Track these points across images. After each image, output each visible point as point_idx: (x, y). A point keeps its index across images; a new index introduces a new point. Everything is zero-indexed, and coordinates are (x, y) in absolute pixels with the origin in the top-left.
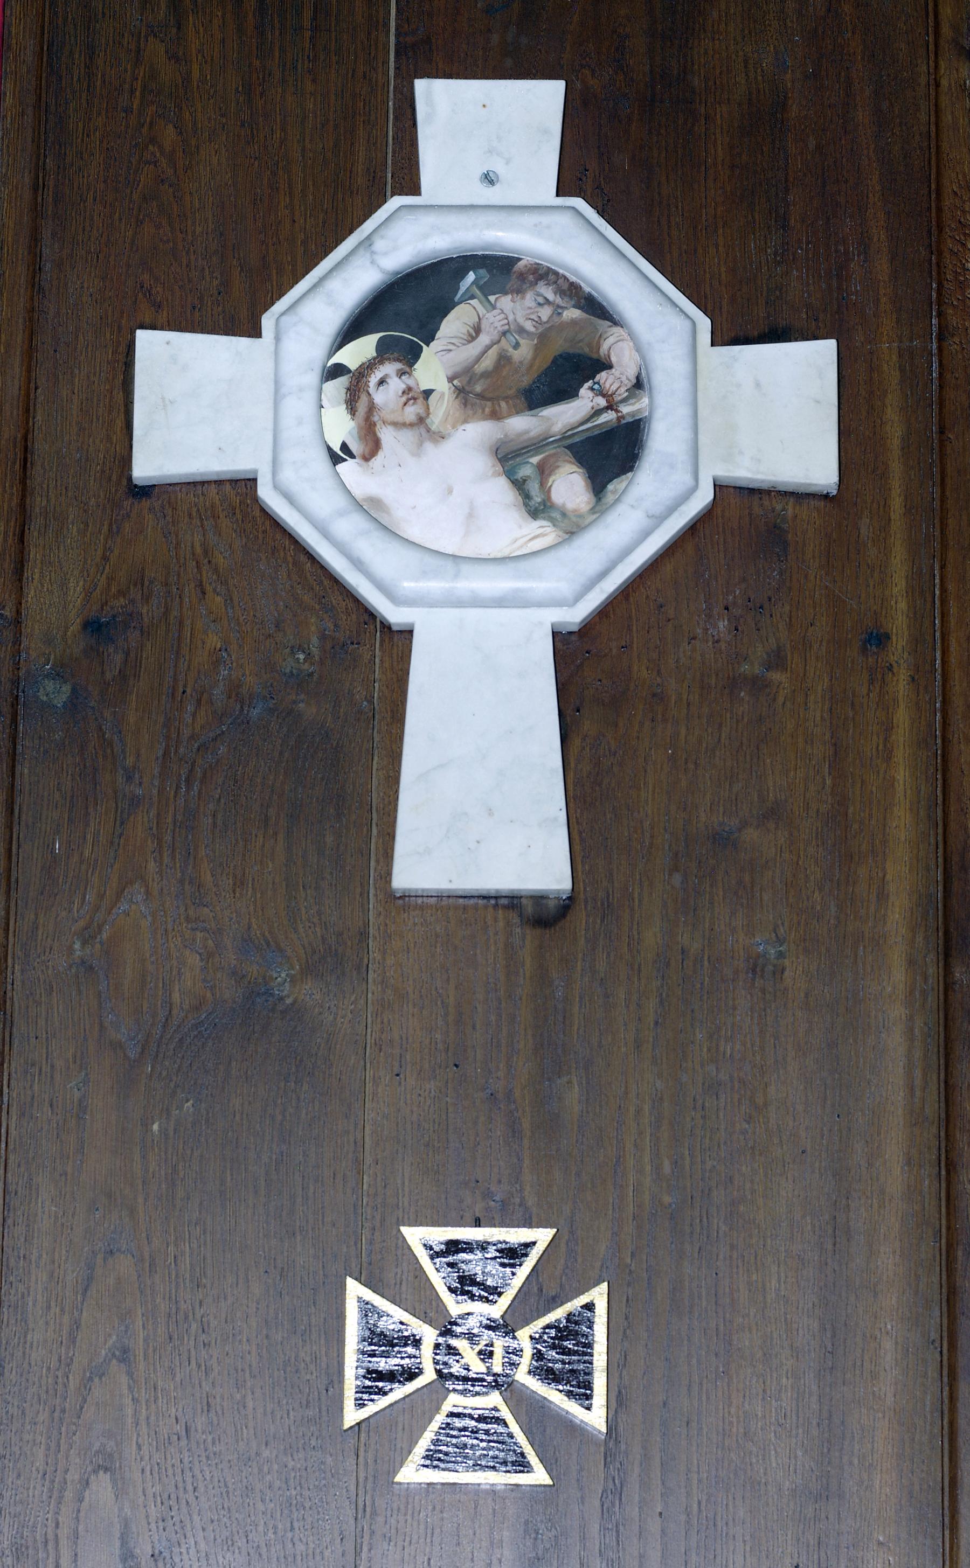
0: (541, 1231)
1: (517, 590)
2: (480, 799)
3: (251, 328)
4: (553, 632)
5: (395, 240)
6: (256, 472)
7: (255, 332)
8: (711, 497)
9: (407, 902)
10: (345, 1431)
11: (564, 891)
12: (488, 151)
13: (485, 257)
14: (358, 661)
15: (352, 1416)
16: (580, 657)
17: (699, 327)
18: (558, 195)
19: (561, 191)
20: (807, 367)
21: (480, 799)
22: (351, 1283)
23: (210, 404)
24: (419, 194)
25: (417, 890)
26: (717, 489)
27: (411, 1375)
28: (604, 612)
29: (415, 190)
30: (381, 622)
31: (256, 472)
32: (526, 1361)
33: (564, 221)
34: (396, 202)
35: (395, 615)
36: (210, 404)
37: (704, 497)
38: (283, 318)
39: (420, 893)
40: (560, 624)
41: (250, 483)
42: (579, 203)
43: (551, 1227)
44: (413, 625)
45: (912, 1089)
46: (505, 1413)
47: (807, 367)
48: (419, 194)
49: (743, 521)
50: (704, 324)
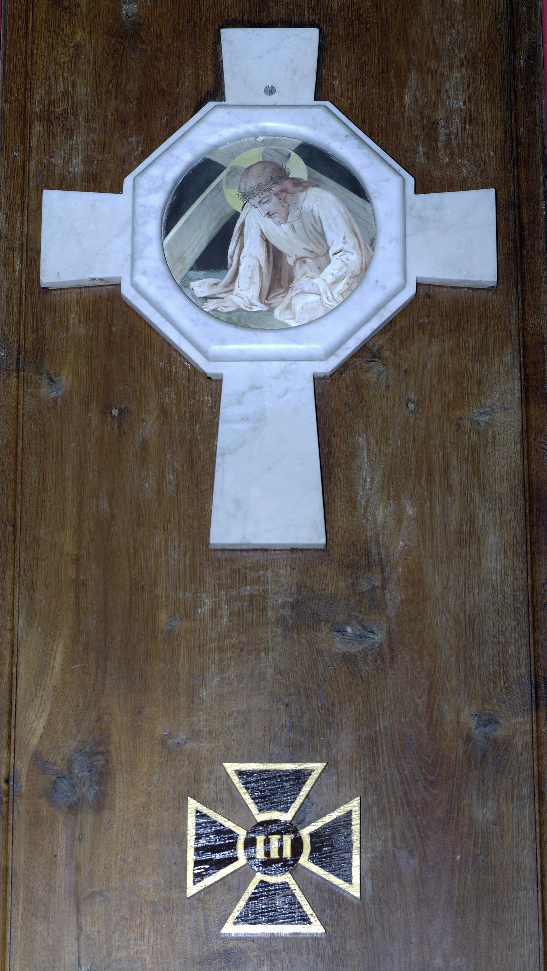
0: (319, 765)
2: (267, 492)
3: (116, 188)
4: (417, 284)
6: (120, 278)
7: (117, 189)
10: (189, 898)
11: (320, 545)
12: (270, 78)
13: (317, 71)
14: (194, 399)
15: (192, 889)
17: (327, 105)
18: (315, 100)
21: (267, 492)
23: (96, 237)
24: (416, 193)
26: (316, 381)
27: (236, 859)
28: (344, 366)
29: (223, 99)
31: (120, 278)
34: (210, 105)
35: (209, 368)
36: (96, 237)
37: (410, 292)
38: (138, 178)
40: (420, 278)
41: (118, 285)
43: (187, 800)
44: (222, 375)
46: (293, 885)
48: (416, 193)
49: (432, 309)
50: (410, 181)
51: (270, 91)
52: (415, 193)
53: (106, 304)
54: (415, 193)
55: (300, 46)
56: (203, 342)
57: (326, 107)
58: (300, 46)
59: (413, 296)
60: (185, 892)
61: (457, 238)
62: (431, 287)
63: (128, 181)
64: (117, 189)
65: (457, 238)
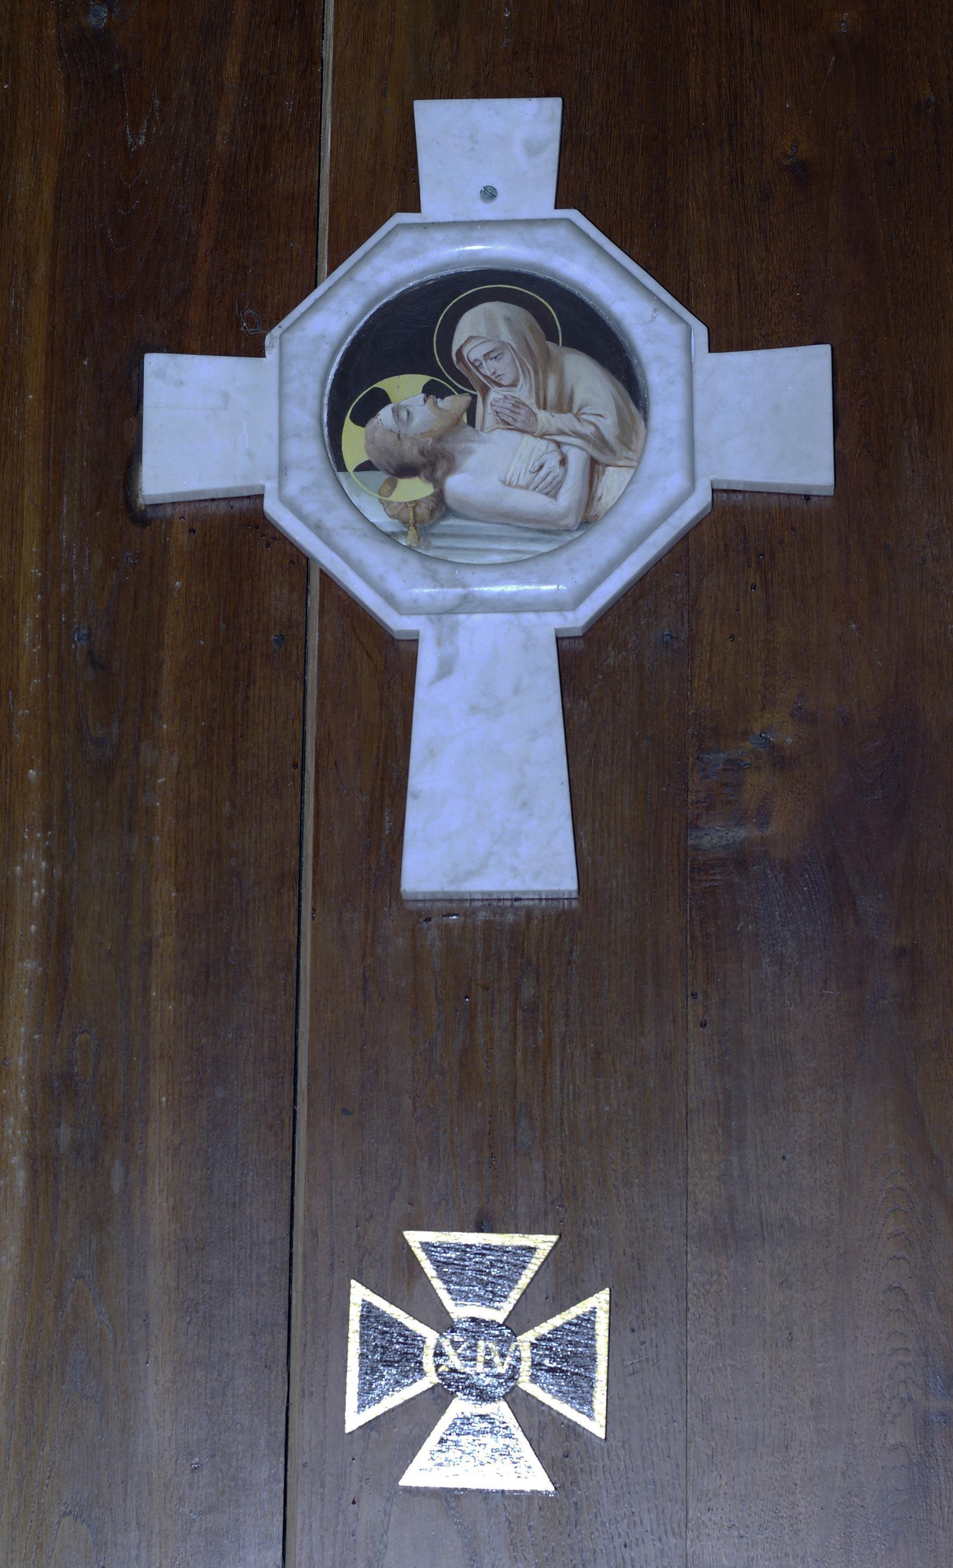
0: (541, 1237)
1: (518, 592)
2: (489, 806)
3: (254, 349)
4: (557, 638)
5: (391, 263)
6: (417, 633)
8: (710, 499)
9: (426, 912)
12: (488, 170)
16: (579, 661)
19: (560, 203)
20: (801, 376)
21: (489, 806)
22: (601, 1433)
23: (211, 425)
25: (416, 893)
29: (415, 207)
30: (321, 571)
31: (417, 633)
32: (525, 1368)
33: (562, 232)
36: (211, 425)
37: (700, 501)
38: (287, 335)
39: (420, 897)
42: (574, 215)
45: (499, 900)
47: (801, 376)
49: (742, 530)
50: (700, 333)
51: (489, 194)
52: (710, 352)
53: (238, 533)
54: (710, 352)
55: (533, 122)
56: (395, 584)
57: (569, 221)
58: (533, 122)
59: (707, 506)
60: (399, 1478)
61: (759, 417)
62: (747, 495)
63: (271, 339)
64: (256, 350)
65: (759, 417)
